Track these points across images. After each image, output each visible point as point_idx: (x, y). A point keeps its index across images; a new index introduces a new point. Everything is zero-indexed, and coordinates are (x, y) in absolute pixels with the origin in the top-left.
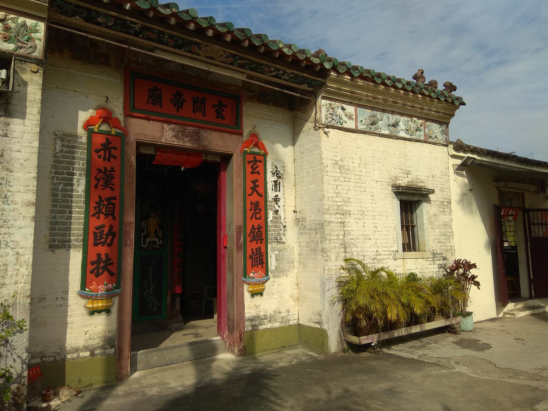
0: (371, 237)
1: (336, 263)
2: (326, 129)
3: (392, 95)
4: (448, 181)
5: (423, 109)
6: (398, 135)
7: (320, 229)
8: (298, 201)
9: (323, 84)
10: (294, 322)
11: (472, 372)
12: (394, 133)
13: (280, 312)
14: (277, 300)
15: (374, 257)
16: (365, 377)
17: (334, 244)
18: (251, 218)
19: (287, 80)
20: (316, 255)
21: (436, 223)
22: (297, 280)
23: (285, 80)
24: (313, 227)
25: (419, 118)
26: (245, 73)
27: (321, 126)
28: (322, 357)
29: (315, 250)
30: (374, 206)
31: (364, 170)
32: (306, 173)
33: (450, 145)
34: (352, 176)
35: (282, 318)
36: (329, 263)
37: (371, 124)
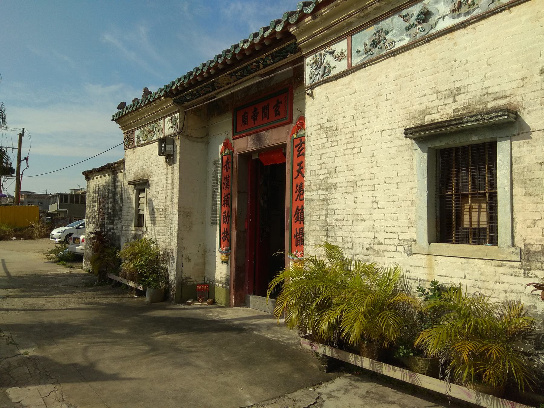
15: (368, 246)
17: (314, 226)
18: (296, 200)
26: (256, 76)
34: (342, 137)
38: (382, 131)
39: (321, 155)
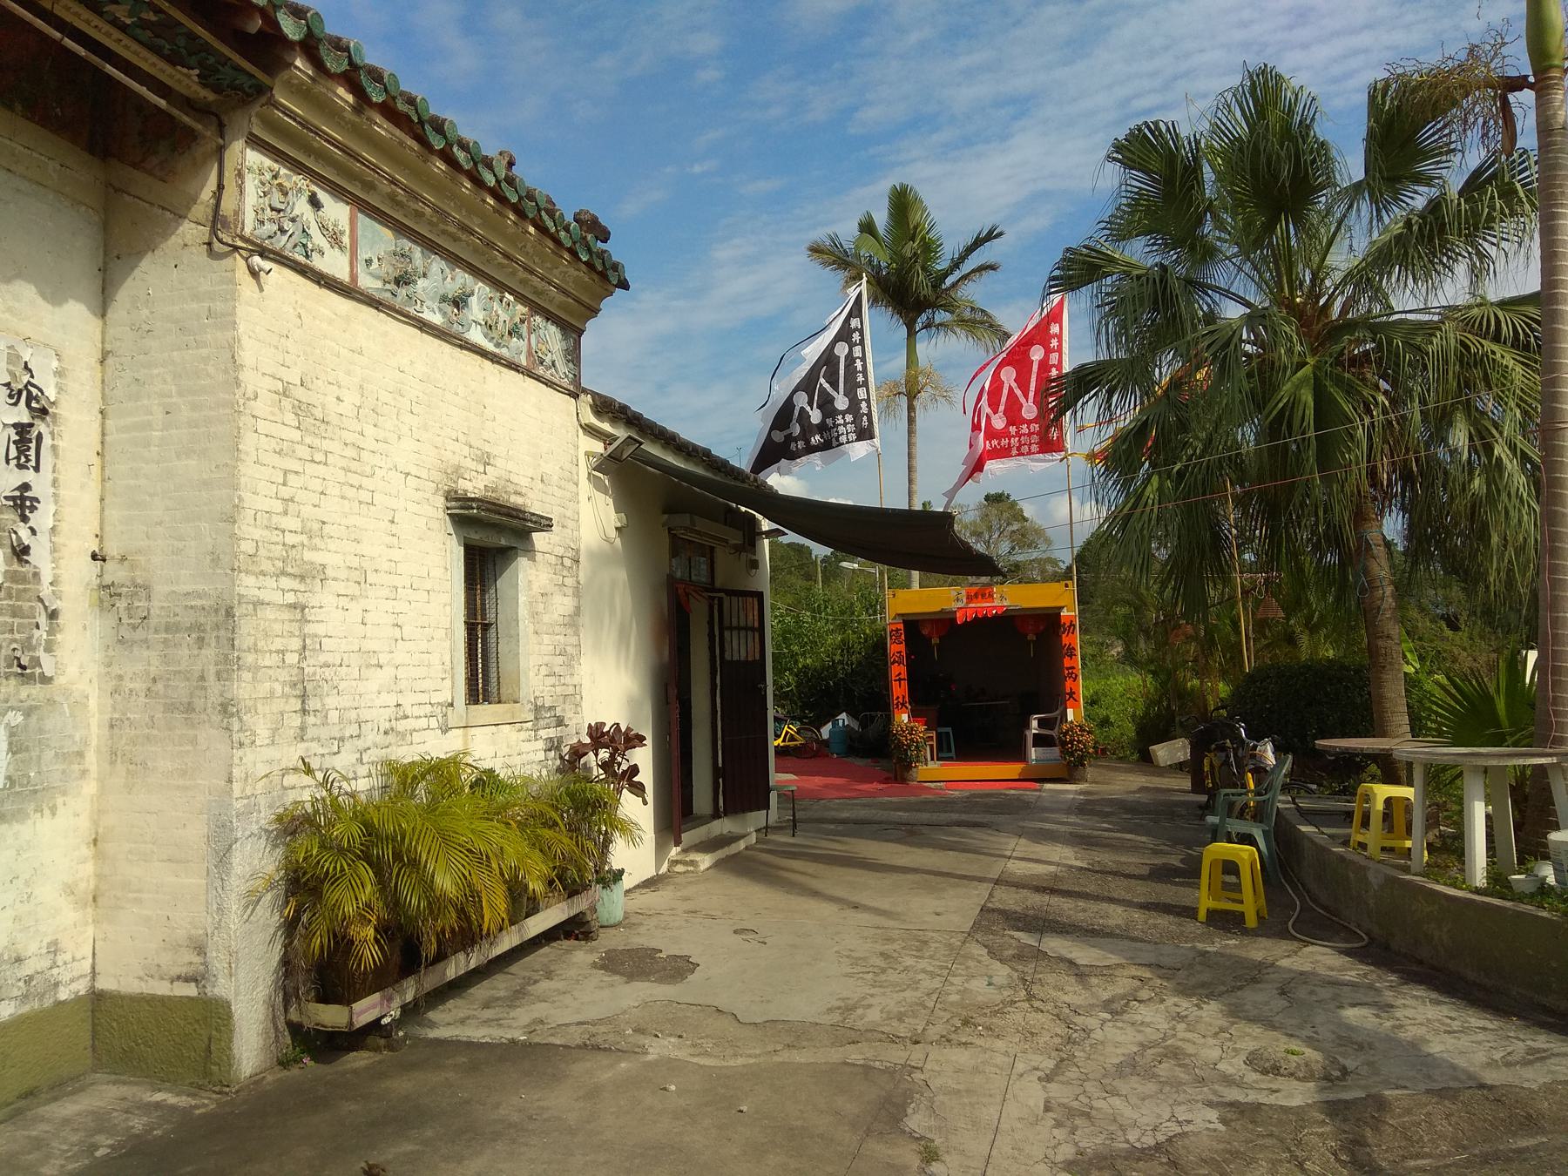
0: (383, 658)
1: (272, 753)
2: (257, 260)
3: (462, 203)
4: (575, 498)
5: (532, 272)
6: (466, 335)
7: (217, 627)
8: (113, 514)
9: (261, 90)
10: (75, 987)
11: (691, 1051)
12: (456, 328)
13: (19, 960)
14: (10, 913)
15: (387, 725)
16: (409, 1147)
19: (123, 28)
20: (193, 726)
21: (546, 619)
22: (96, 823)
23: (115, 23)
24: (187, 619)
25: (521, 298)
27: (239, 243)
28: (205, 1103)
29: (190, 708)
30: (396, 554)
31: (370, 431)
32: (159, 415)
33: (582, 396)
34: (334, 446)
35: (29, 980)
36: (249, 755)
37: (397, 282)
38: (408, 474)
39: (286, 472)
